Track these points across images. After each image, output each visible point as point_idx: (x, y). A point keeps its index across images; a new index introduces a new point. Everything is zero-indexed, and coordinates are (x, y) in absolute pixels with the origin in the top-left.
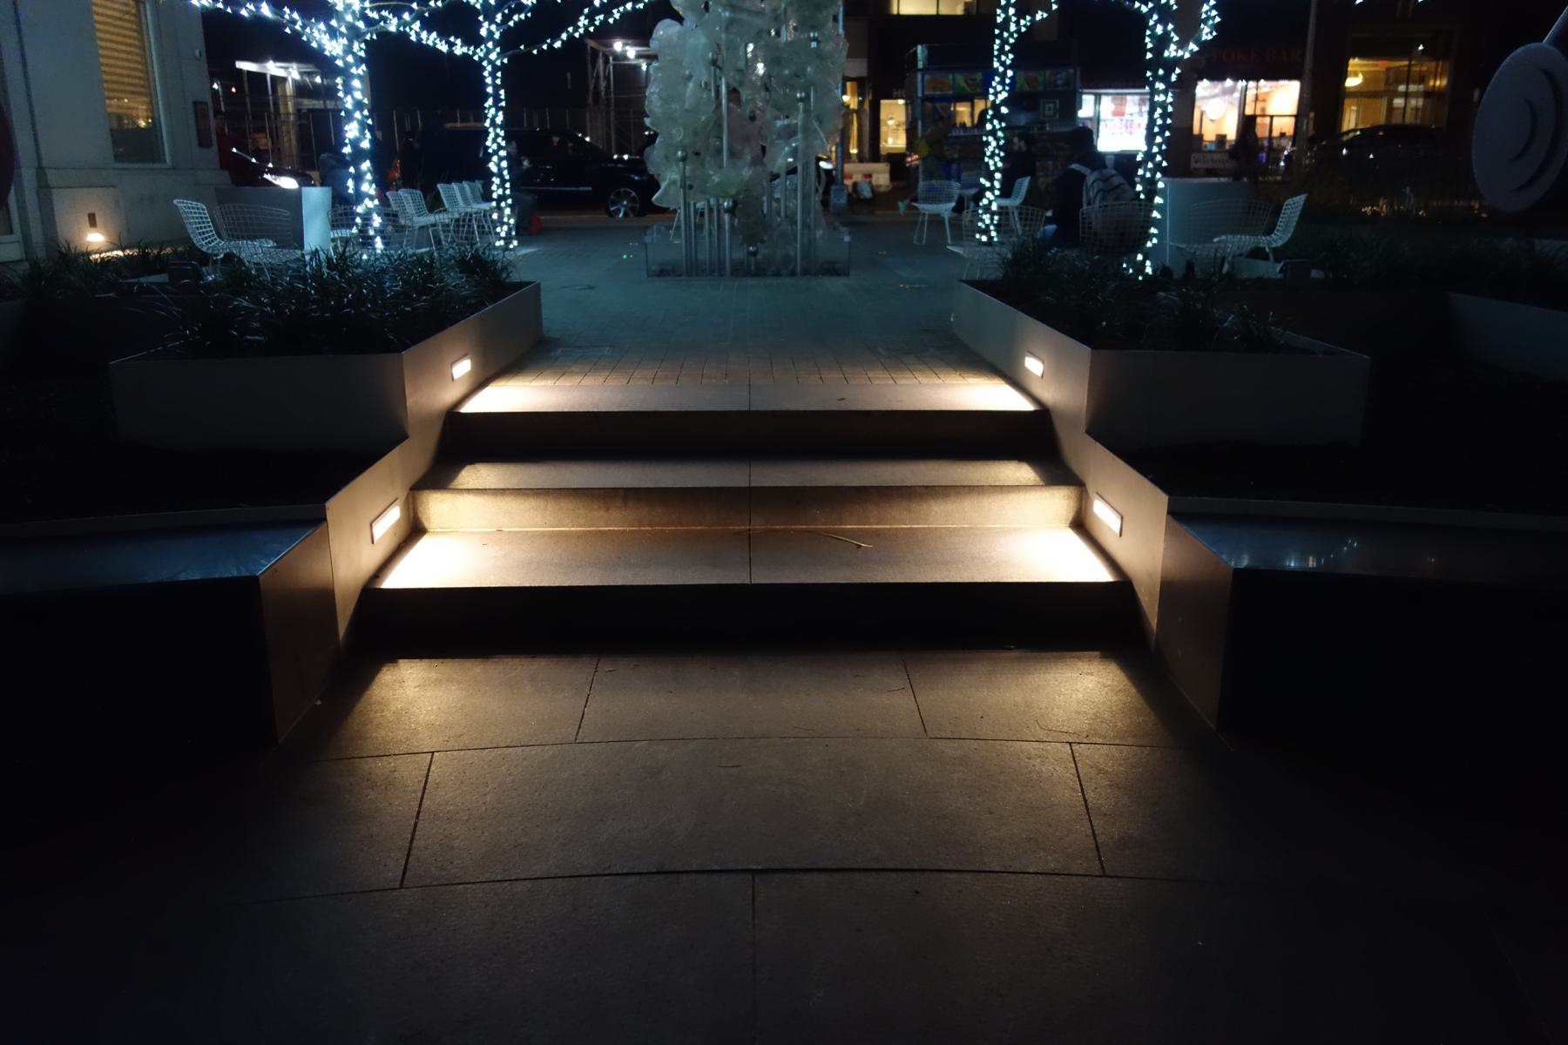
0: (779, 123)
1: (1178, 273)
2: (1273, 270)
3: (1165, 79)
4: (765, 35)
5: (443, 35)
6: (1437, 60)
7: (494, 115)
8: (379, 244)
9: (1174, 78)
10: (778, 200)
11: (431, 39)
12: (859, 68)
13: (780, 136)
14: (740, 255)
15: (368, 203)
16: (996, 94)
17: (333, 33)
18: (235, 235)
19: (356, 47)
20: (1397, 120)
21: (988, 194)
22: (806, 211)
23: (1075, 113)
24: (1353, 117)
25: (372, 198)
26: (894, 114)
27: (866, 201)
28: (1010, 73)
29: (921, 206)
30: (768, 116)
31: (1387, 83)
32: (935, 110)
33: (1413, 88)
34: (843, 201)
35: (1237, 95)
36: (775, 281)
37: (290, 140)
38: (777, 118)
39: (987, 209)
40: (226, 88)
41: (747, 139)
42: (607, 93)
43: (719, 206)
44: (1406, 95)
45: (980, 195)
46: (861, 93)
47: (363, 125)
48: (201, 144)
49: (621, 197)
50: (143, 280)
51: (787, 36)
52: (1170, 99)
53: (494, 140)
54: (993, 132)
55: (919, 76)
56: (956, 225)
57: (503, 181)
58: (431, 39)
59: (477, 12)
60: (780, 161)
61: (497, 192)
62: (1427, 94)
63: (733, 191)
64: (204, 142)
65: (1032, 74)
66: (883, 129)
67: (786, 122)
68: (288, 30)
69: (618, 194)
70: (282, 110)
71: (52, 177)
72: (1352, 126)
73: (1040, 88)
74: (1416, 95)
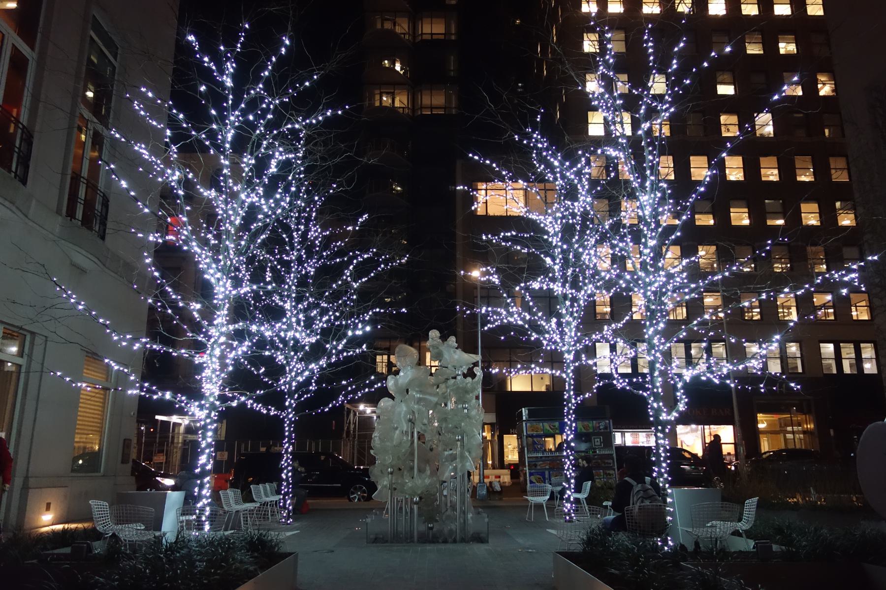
0: (446, 453)
1: (690, 548)
2: (748, 545)
3: (663, 431)
4: (439, 407)
5: (265, 405)
6: (805, 414)
7: (288, 447)
8: (207, 527)
9: (667, 430)
10: (445, 496)
11: (258, 407)
12: (492, 418)
13: (447, 461)
14: (423, 528)
15: (205, 501)
16: (568, 436)
17: (201, 407)
18: (119, 521)
19: (213, 414)
20: (791, 446)
21: (568, 492)
22: (463, 502)
24: (766, 444)
25: (207, 498)
26: (511, 443)
27: (497, 492)
28: (574, 425)
29: (529, 498)
30: (440, 449)
31: (781, 426)
32: (534, 443)
33: (795, 428)
34: (484, 492)
35: (699, 432)
36: (442, 547)
37: (177, 457)
38: (445, 450)
39: (568, 500)
40: (147, 429)
41: (427, 461)
42: (355, 428)
43: (412, 499)
44: (793, 432)
45: (563, 492)
46: (493, 430)
47: (209, 456)
48: (122, 462)
50: (56, 551)
51: (451, 406)
52: (667, 443)
53: (286, 460)
54: (568, 457)
56: (551, 509)
57: (289, 484)
58: (258, 407)
59: (285, 394)
60: (447, 474)
61: (284, 490)
62: (805, 432)
63: (419, 492)
64: (124, 461)
65: (586, 423)
66: (505, 450)
67: (451, 452)
70: (176, 441)
71: (32, 481)
72: (767, 450)
73: (591, 431)
74: (799, 432)
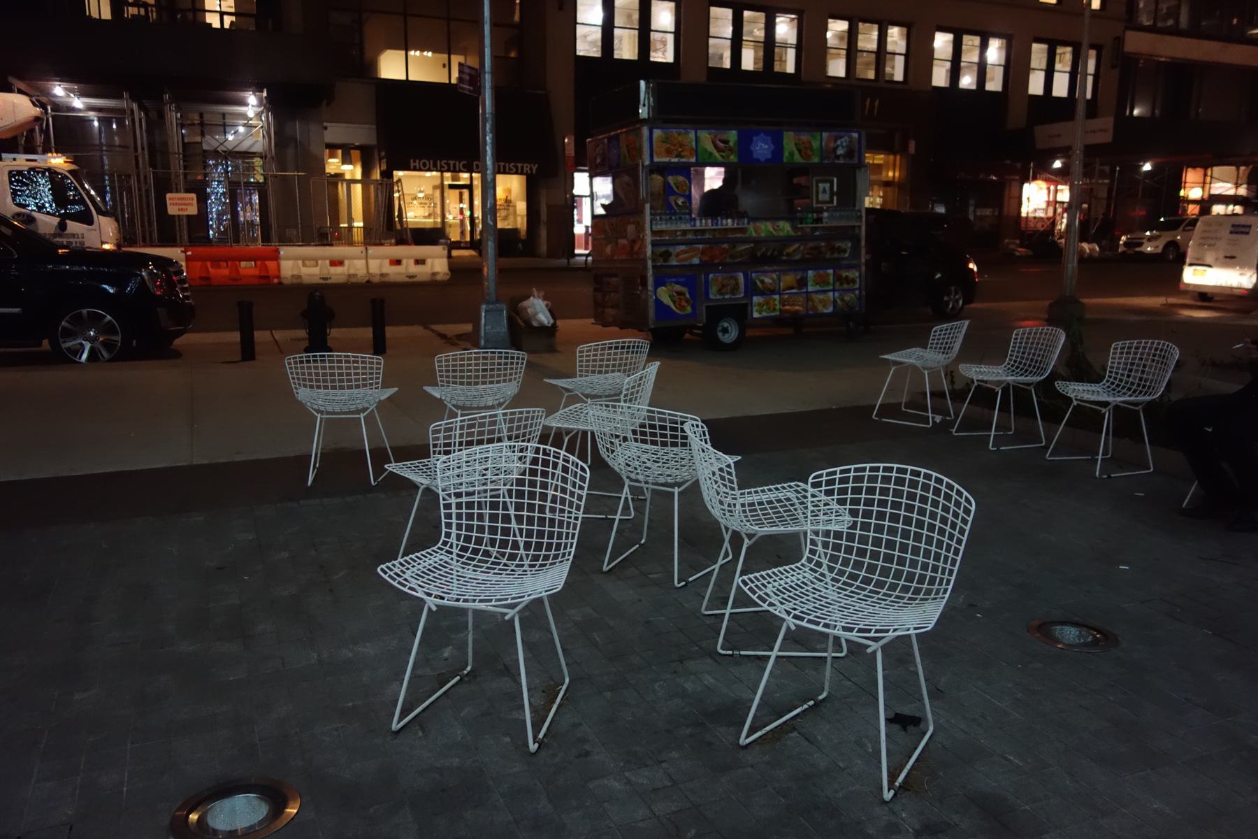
23: (324, 169)
49: (80, 326)
55: (645, 131)
65: (804, 137)
68: (946, 298)
69: (78, 319)
73: (816, 160)
